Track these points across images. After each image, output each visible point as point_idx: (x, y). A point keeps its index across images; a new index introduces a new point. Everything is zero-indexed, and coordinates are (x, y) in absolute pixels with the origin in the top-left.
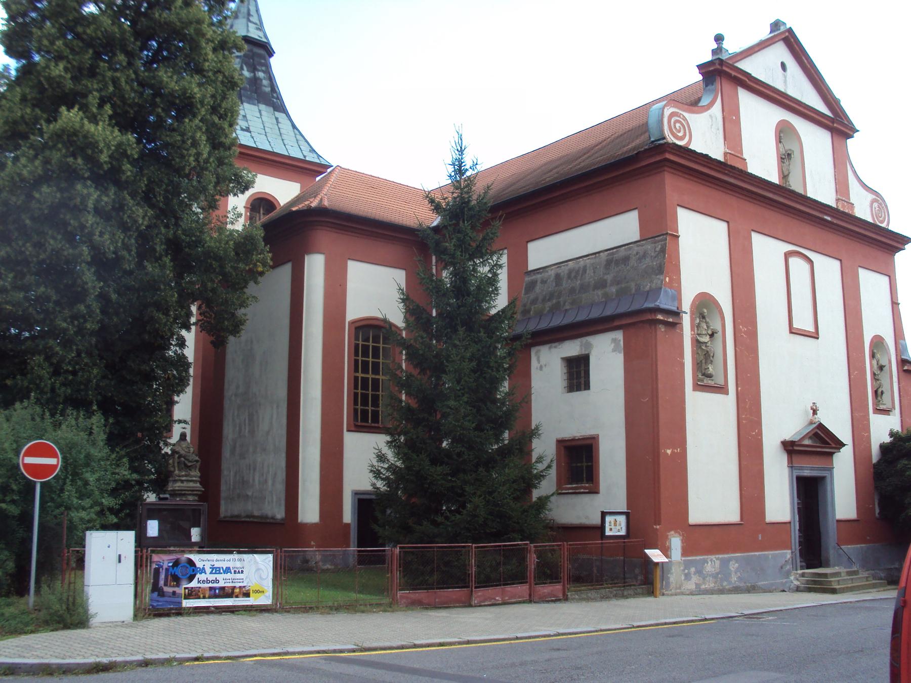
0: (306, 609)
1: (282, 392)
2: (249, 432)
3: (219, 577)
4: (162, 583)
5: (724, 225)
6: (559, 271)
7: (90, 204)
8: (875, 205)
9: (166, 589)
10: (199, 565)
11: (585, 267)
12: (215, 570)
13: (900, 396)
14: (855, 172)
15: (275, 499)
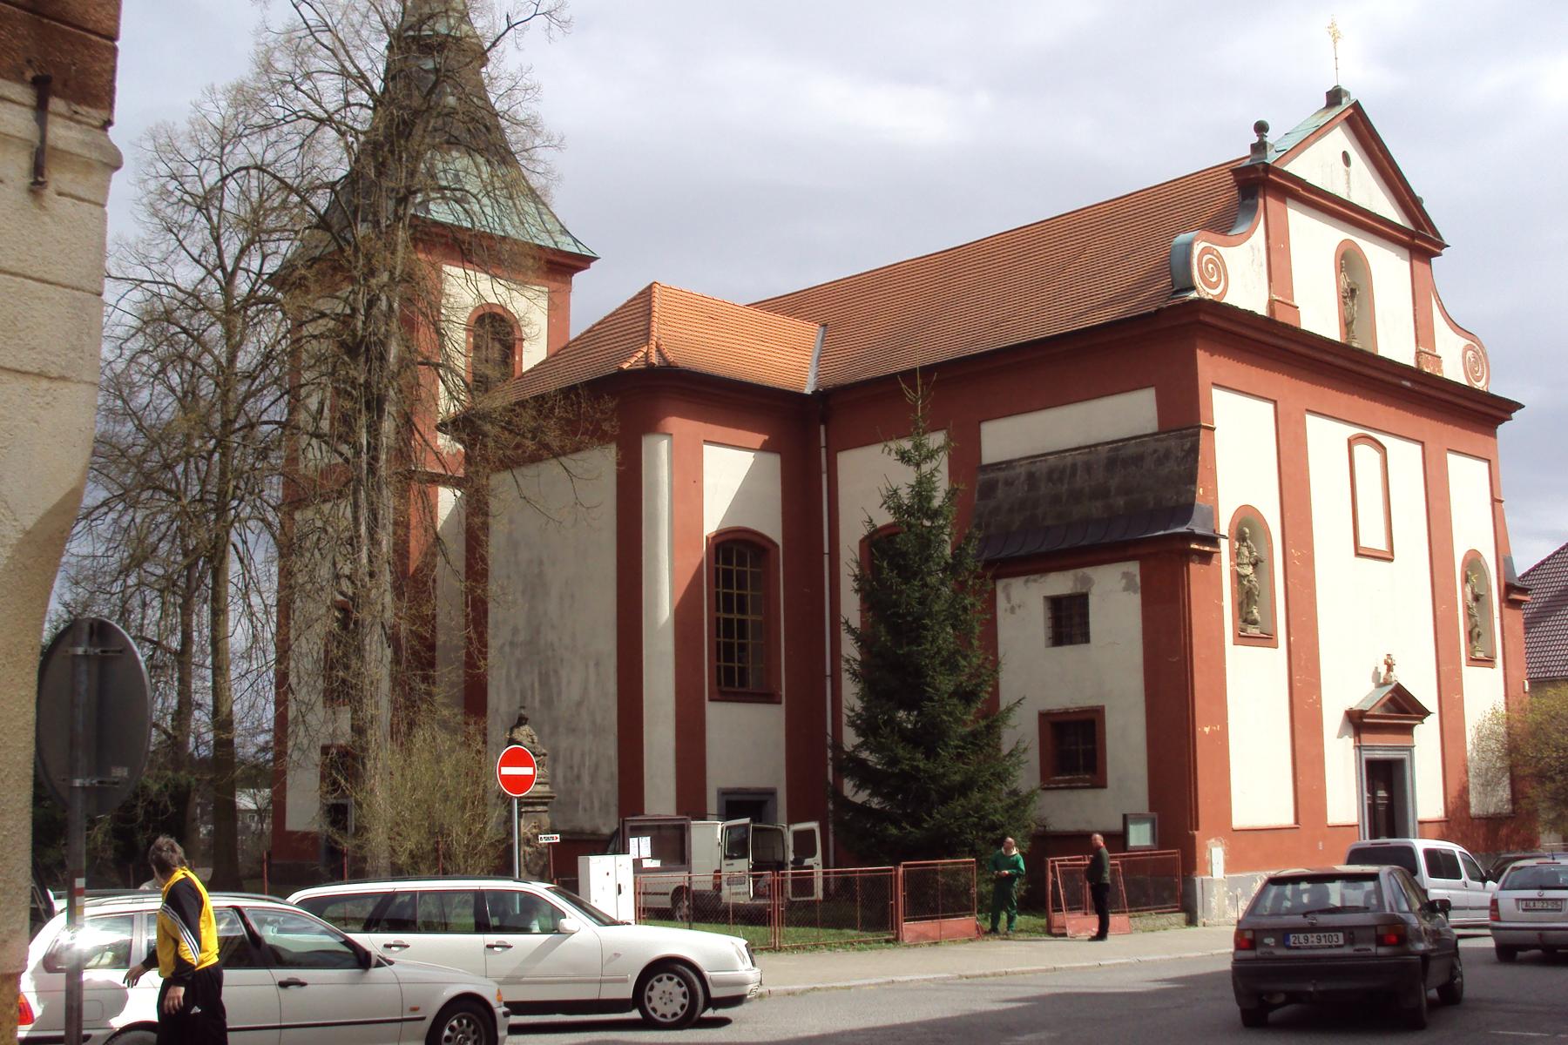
2: (541, 701)
5: (1268, 408)
8: (1470, 353)
11: (1074, 466)
15: (596, 804)
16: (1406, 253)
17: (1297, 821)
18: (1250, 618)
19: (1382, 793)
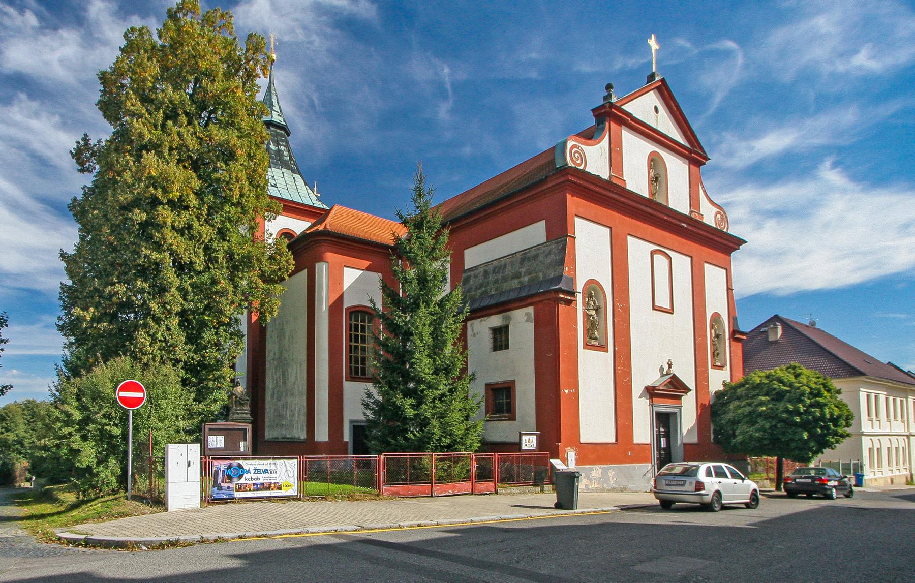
0: (323, 497)
1: (303, 356)
3: (259, 476)
4: (220, 480)
6: (487, 268)
7: (169, 224)
8: (719, 216)
9: (223, 485)
10: (246, 467)
11: (505, 264)
12: (257, 471)
13: (731, 356)
16: (687, 161)
17: (617, 441)
19: (662, 429)
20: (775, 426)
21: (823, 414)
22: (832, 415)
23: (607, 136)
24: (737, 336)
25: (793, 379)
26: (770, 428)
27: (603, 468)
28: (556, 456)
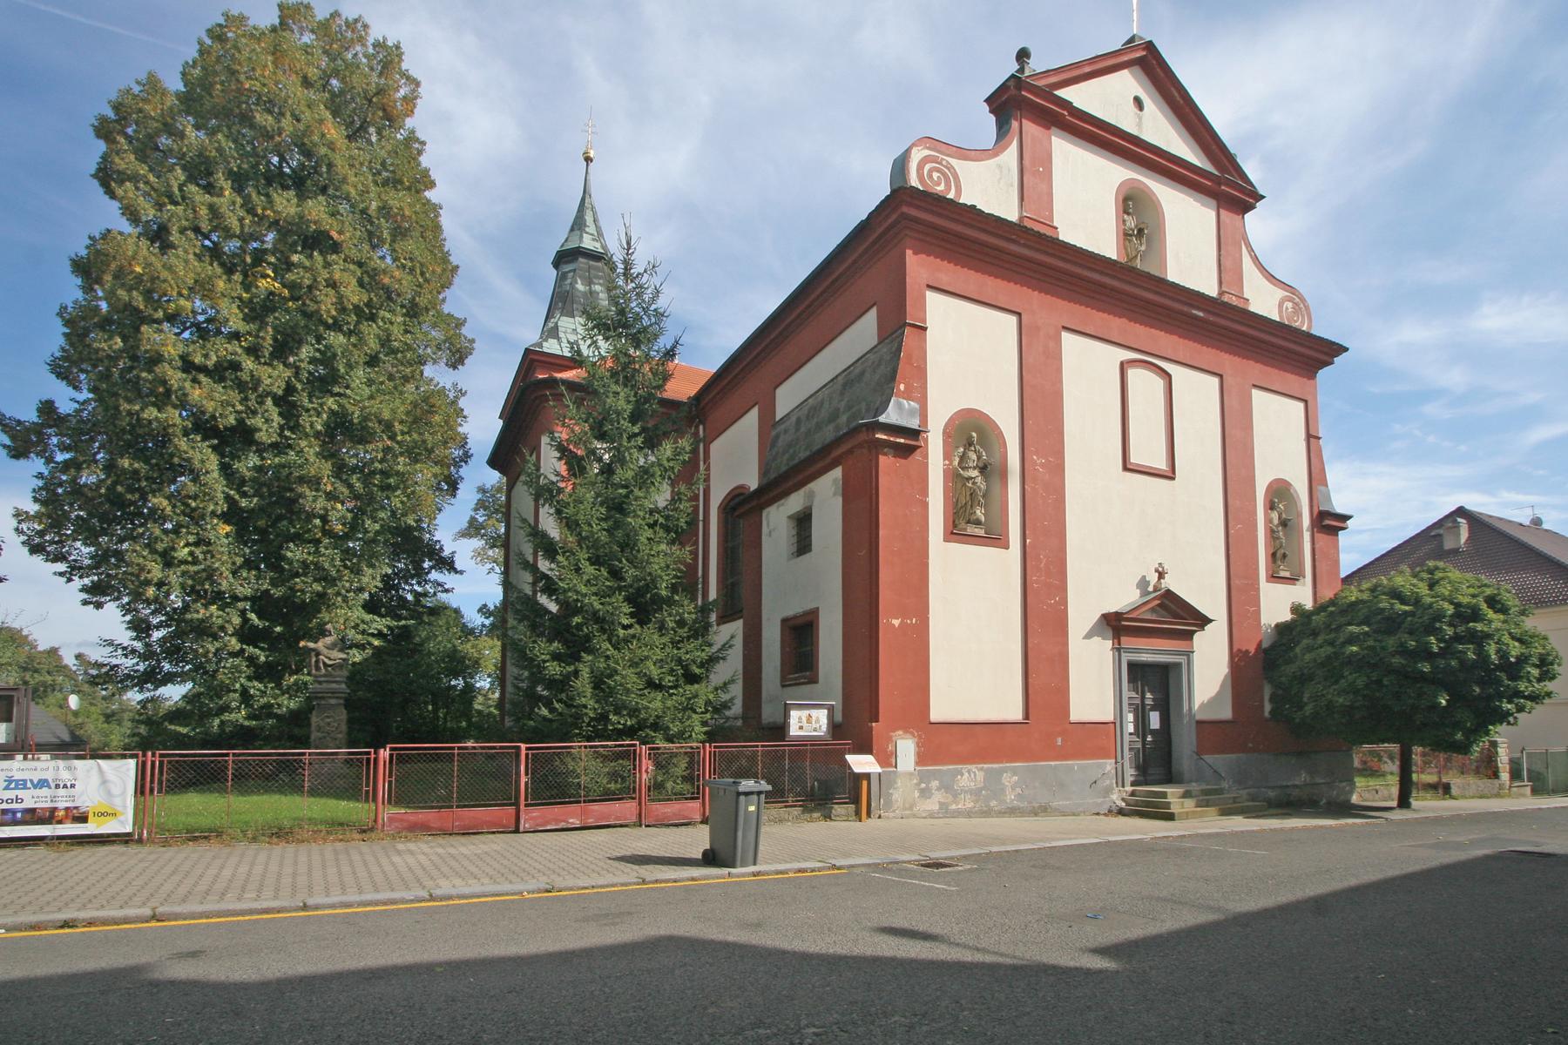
14: (1255, 259)
16: (1214, 203)
17: (1027, 715)
18: (973, 518)
20: (1379, 682)
21: (1483, 657)
22: (1503, 655)
23: (1015, 143)
24: (1327, 522)
25: (1423, 589)
26: (1367, 686)
27: (987, 771)
28: (864, 748)
